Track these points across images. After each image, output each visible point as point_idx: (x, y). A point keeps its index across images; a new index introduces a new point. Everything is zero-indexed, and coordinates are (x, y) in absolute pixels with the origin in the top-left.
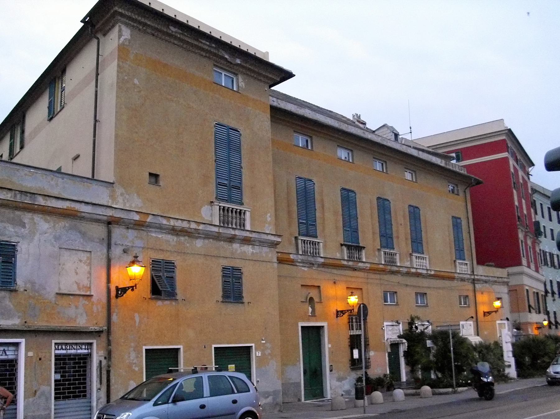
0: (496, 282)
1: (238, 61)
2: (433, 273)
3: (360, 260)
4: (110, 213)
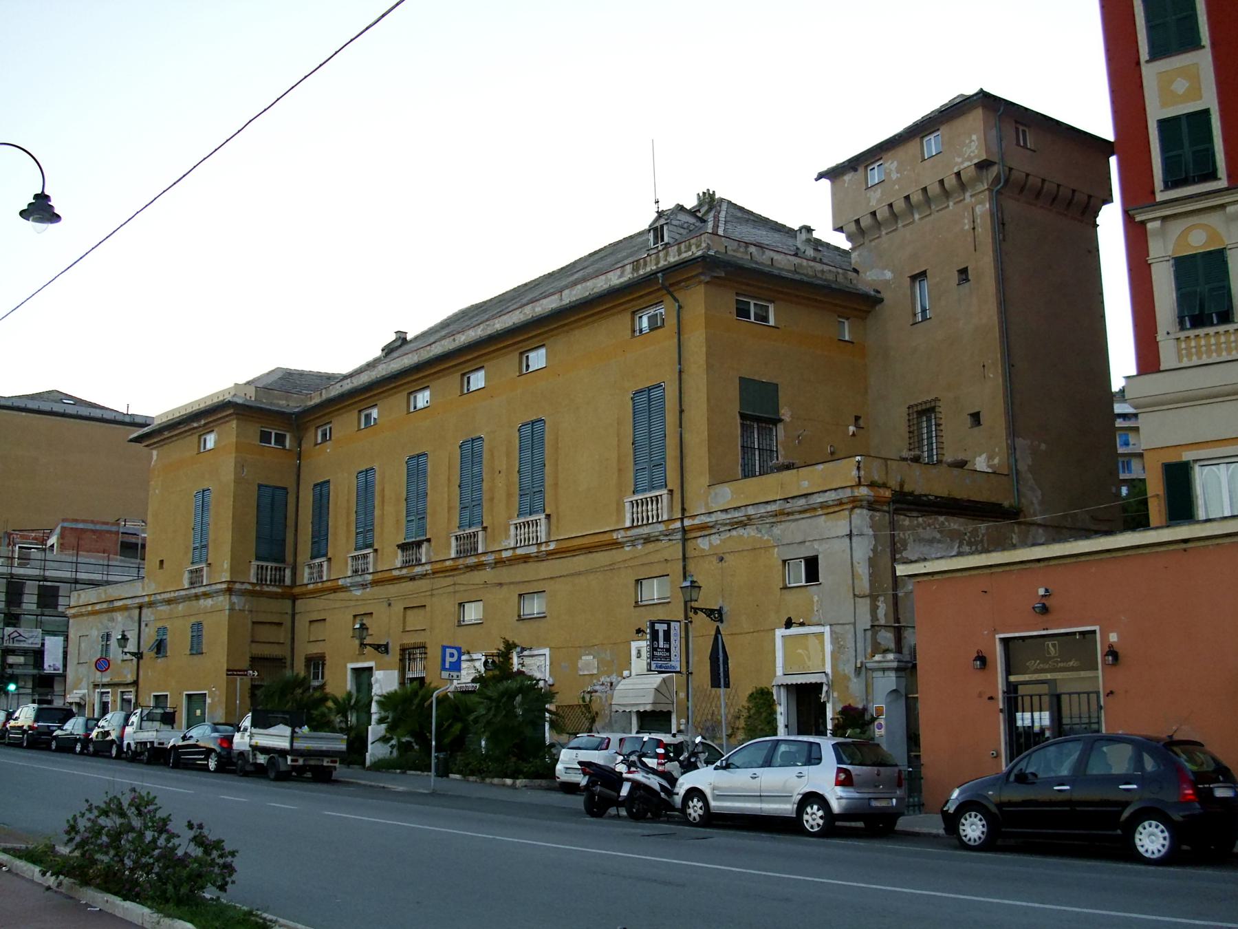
0: (782, 513)
1: (203, 422)
2: (552, 546)
3: (419, 563)
4: (137, 601)
